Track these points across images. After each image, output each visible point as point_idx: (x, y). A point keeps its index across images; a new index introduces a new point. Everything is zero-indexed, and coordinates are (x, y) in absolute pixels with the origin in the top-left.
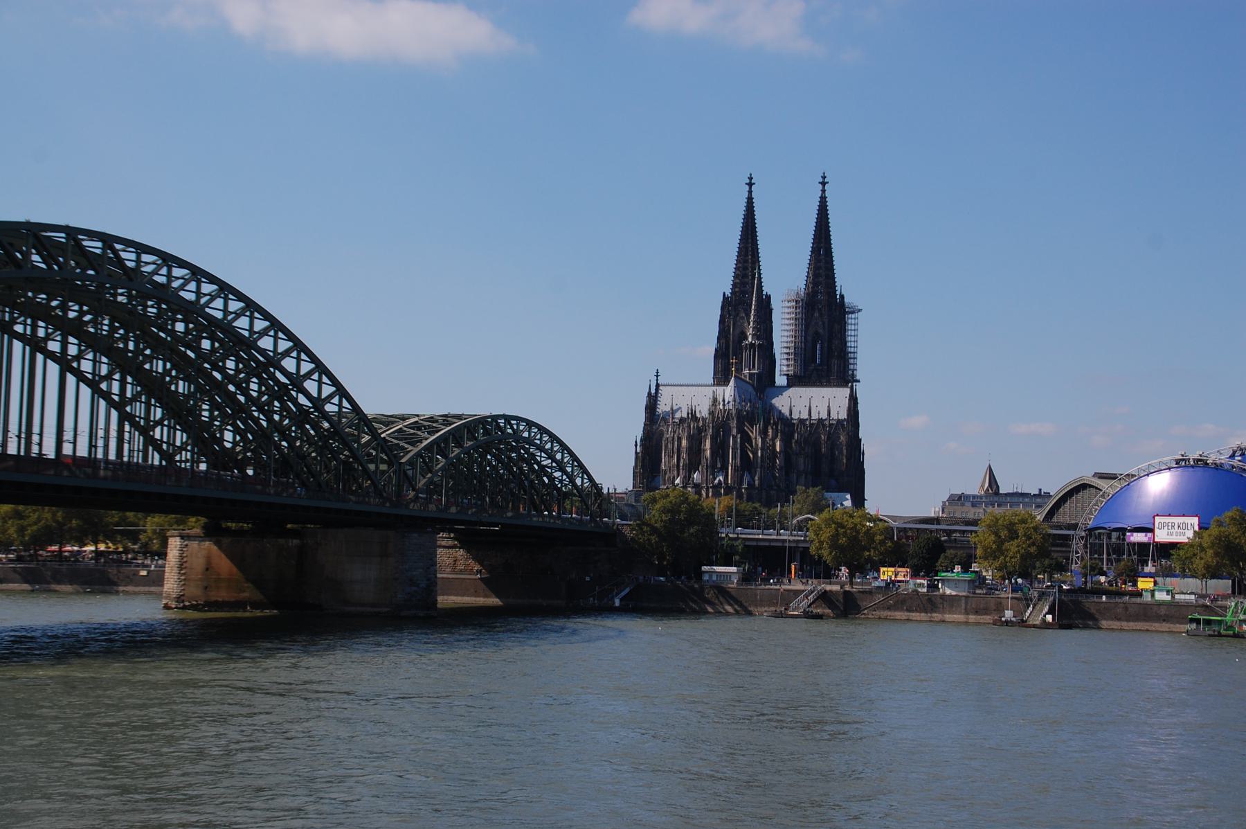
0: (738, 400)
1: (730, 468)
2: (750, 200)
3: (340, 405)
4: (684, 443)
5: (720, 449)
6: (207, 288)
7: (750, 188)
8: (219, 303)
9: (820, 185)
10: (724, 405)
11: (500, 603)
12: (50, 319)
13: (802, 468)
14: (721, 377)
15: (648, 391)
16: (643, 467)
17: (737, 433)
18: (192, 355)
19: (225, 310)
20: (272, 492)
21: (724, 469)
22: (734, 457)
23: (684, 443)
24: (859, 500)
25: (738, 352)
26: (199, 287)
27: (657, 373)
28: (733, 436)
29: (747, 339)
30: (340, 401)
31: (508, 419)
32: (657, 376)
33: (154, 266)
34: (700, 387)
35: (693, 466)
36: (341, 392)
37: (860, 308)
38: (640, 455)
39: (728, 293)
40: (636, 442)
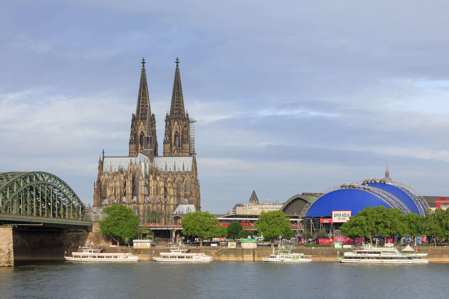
7: (143, 65)
27: (103, 151)
34: (113, 158)
37: (195, 120)
39: (135, 113)
40: (95, 184)
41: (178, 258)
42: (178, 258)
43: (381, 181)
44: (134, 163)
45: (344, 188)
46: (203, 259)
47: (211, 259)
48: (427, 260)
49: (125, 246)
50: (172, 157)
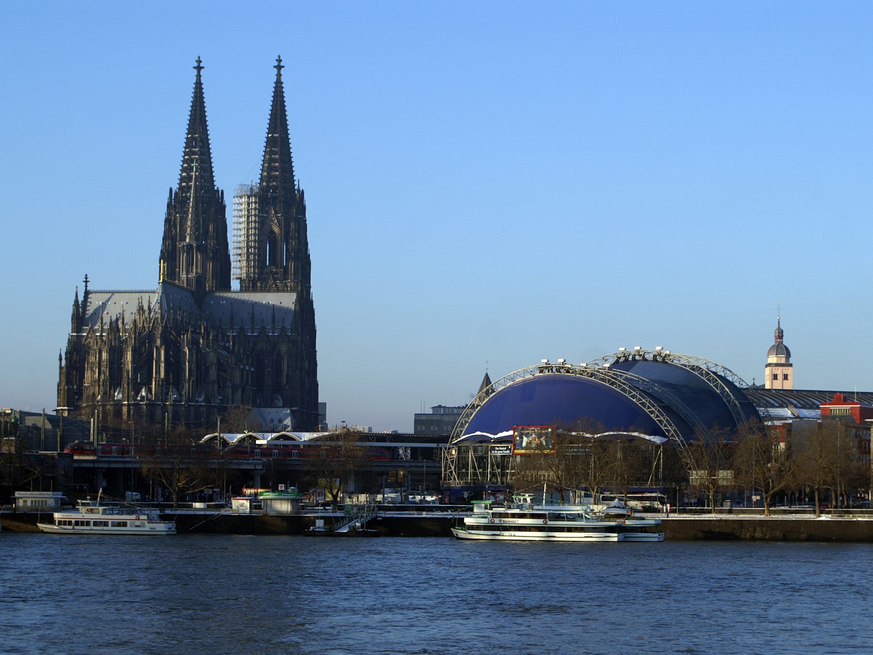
1: (154, 383)
2: (199, 86)
4: (104, 355)
5: (143, 362)
9: (275, 69)
10: (150, 313)
11: (39, 525)
15: (74, 298)
16: (67, 383)
17: (161, 345)
27: (86, 278)
28: (157, 348)
29: (185, 240)
32: (86, 282)
34: (104, 294)
35: (115, 379)
38: (64, 370)
39: (175, 187)
40: (60, 356)
41: (94, 525)
42: (94, 525)
43: (635, 355)
44: (146, 308)
45: (546, 373)
46: (151, 528)
47: (169, 529)
48: (616, 535)
49: (101, 505)
50: (254, 294)
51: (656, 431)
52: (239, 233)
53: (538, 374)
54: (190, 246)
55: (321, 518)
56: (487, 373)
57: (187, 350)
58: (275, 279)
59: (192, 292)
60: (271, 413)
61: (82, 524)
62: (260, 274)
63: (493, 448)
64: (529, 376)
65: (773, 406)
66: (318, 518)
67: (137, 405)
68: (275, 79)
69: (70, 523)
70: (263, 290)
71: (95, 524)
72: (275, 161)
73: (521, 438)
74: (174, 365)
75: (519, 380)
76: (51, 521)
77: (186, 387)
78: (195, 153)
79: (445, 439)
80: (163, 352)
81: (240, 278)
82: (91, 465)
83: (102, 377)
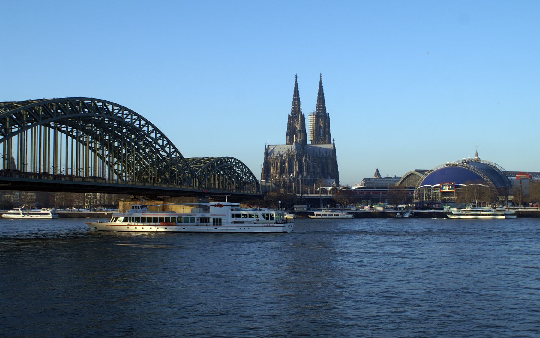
0: (296, 149)
2: (296, 83)
3: (176, 155)
4: (279, 164)
5: (291, 166)
6: (134, 117)
8: (138, 122)
11: (309, 216)
12: (83, 130)
13: (318, 171)
14: (290, 141)
16: (264, 173)
17: (297, 160)
18: (128, 140)
19: (140, 125)
20: (309, 177)
21: (292, 172)
22: (296, 169)
23: (279, 164)
24: (337, 181)
25: (295, 133)
26: (132, 117)
30: (176, 154)
31: (228, 158)
32: (268, 142)
33: (118, 111)
35: (283, 171)
36: (176, 150)
39: (290, 114)
44: (291, 150)
45: (449, 166)
48: (504, 216)
51: (486, 183)
52: (310, 127)
53: (446, 166)
54: (300, 131)
55: (399, 212)
56: (377, 169)
57: (304, 162)
58: (322, 140)
59: (301, 145)
60: (329, 181)
61: (324, 215)
62: (317, 139)
63: (433, 190)
64: (442, 167)
65: (512, 177)
66: (398, 212)
67: (290, 179)
68: (320, 80)
69: (320, 215)
70: (318, 144)
71: (334, 215)
72: (321, 104)
73: (443, 187)
74: (300, 167)
75: (439, 168)
76: (313, 214)
77: (304, 174)
78: (296, 103)
79: (414, 188)
80: (297, 163)
81: (311, 141)
82: (325, 197)
83: (278, 171)
